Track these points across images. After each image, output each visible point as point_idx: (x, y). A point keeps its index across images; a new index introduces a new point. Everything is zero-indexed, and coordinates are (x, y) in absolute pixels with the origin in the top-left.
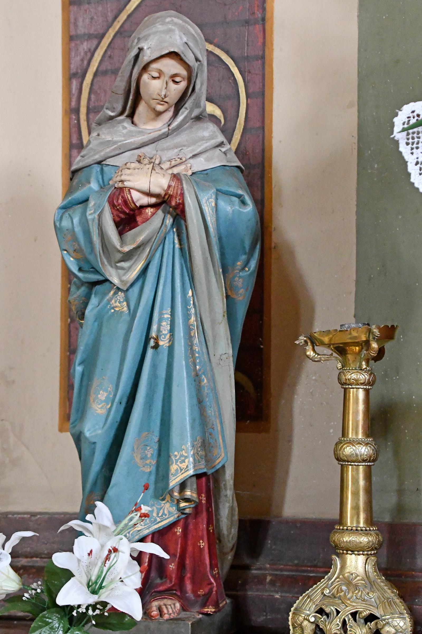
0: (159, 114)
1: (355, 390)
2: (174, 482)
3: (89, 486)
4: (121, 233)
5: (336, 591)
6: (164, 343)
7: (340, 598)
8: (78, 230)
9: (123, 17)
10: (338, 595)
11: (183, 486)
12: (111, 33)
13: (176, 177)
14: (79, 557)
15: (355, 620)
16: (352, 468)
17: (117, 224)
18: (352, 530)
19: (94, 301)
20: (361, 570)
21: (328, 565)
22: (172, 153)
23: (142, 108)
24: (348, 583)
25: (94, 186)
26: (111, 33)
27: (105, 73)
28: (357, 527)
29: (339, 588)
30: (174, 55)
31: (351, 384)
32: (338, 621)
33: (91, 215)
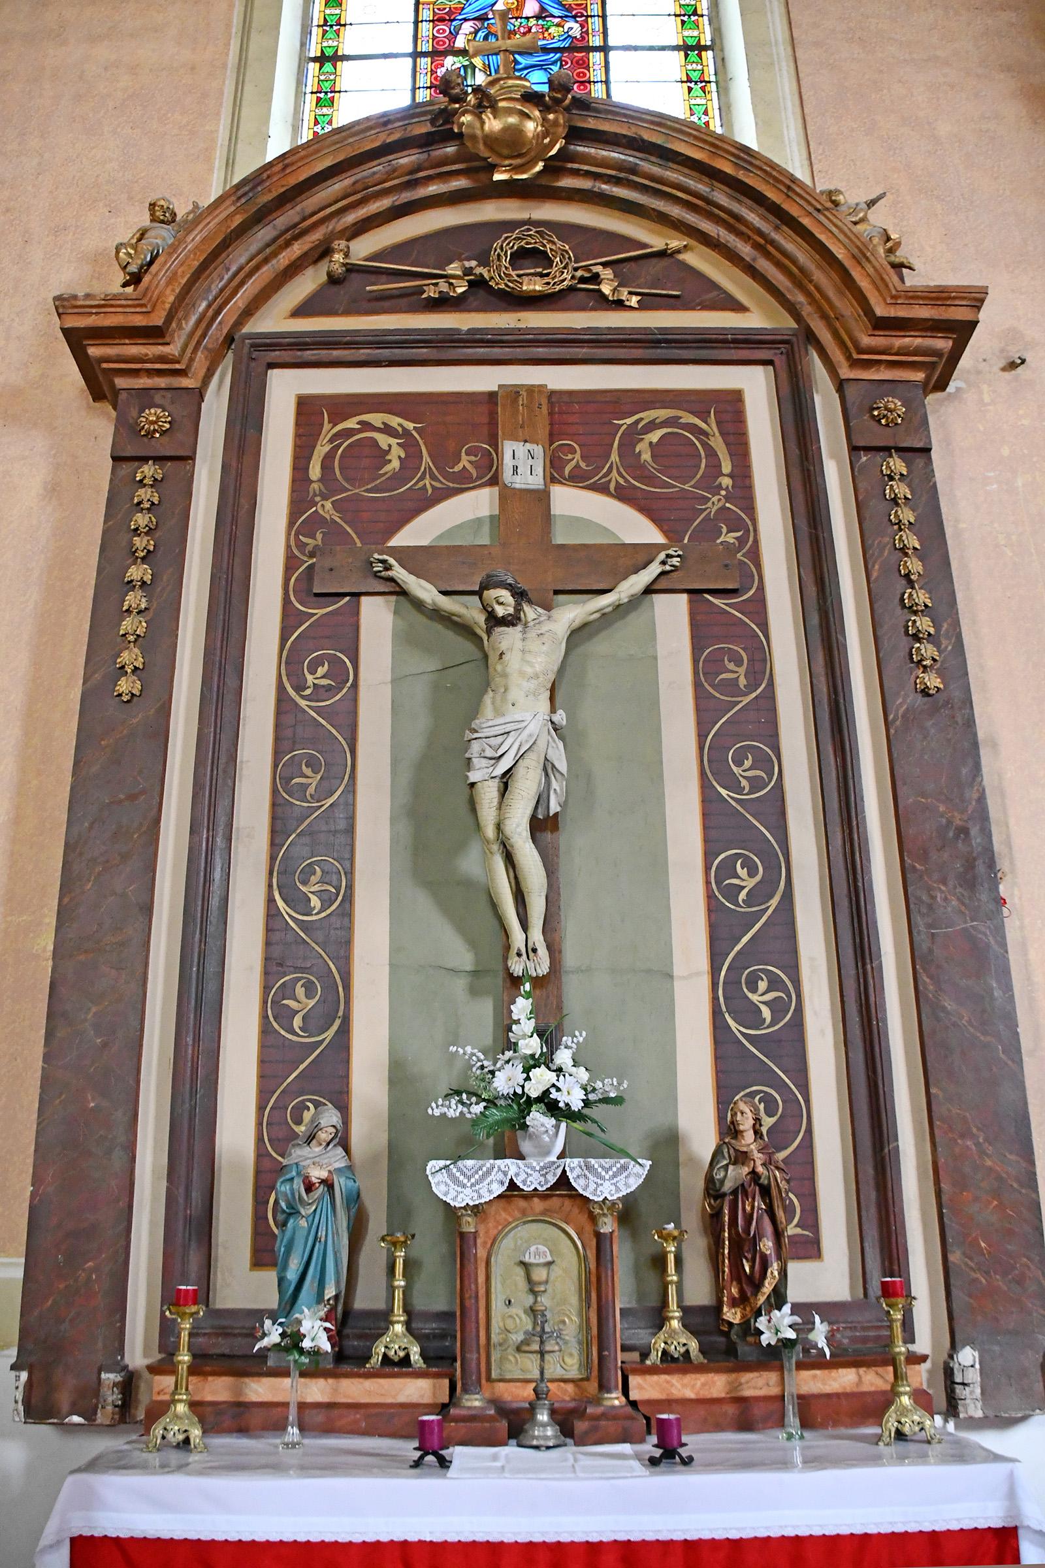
0: (321, 1144)
2: (326, 1298)
3: (284, 1303)
4: (307, 1193)
6: (323, 1240)
8: (288, 1192)
9: (285, 1084)
11: (329, 1300)
12: (279, 1092)
13: (330, 1171)
17: (306, 1190)
19: (291, 1221)
20: (400, 1331)
21: (388, 1329)
22: (326, 1161)
23: (314, 1142)
24: (397, 1335)
25: (294, 1173)
26: (279, 1092)
27: (275, 1108)
30: (333, 1126)
33: (295, 1186)
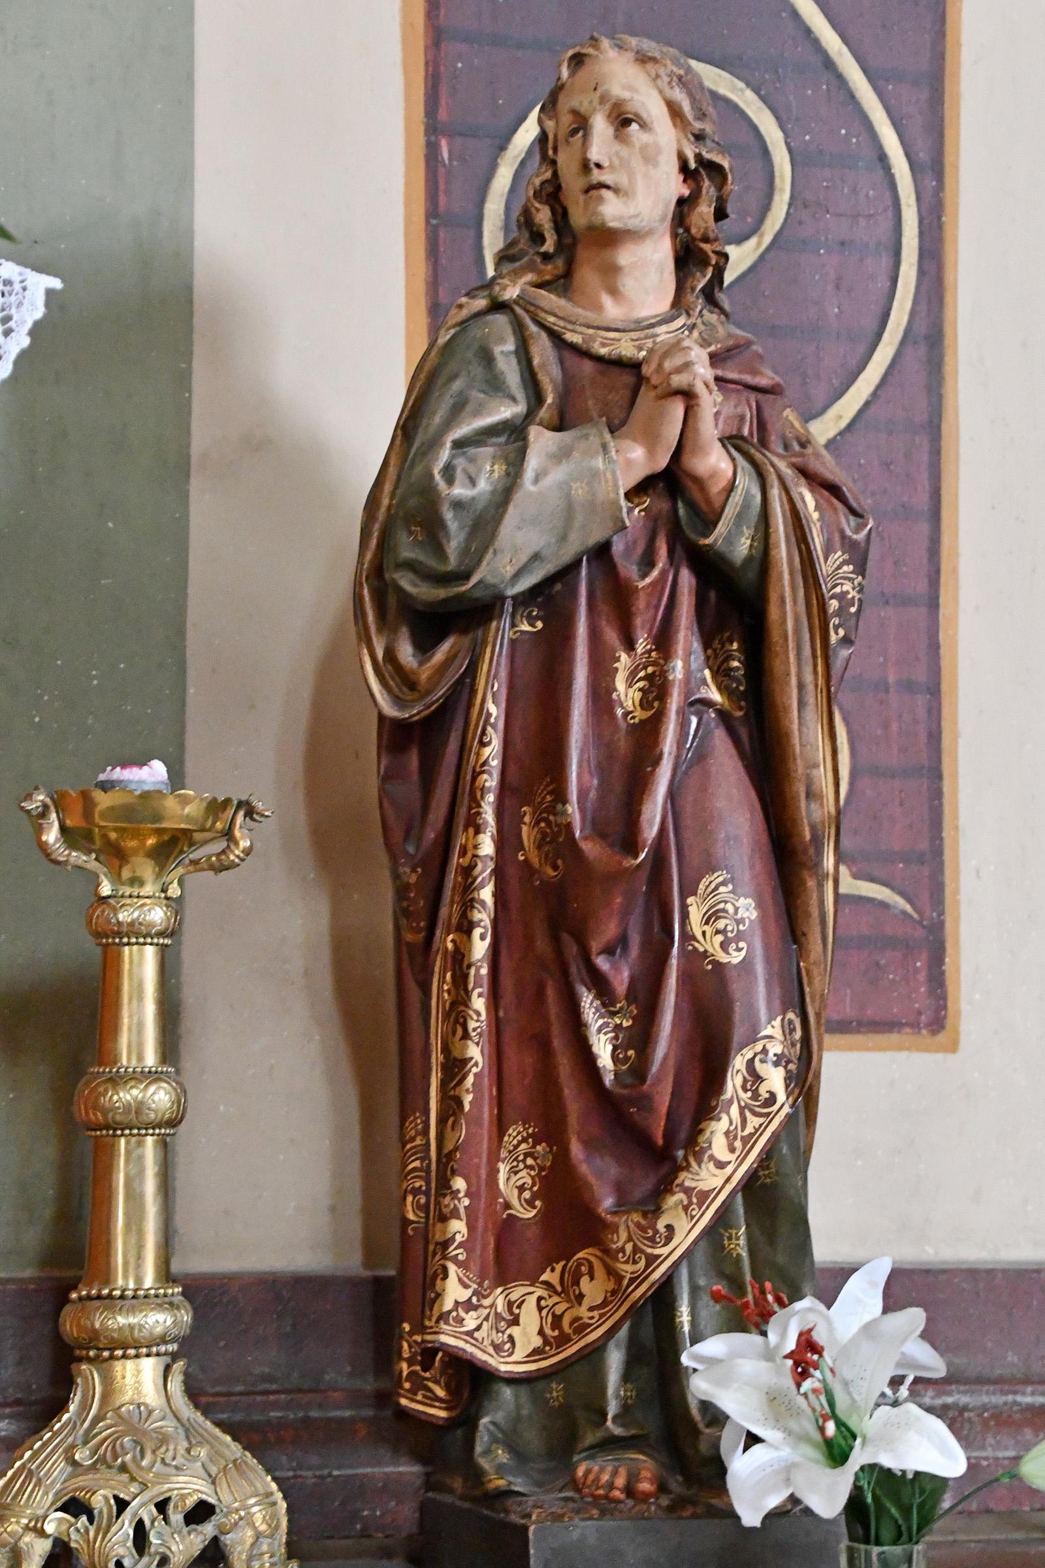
1: (135, 948)
5: (110, 1448)
7: (123, 1468)
10: (120, 1460)
14: (683, 1214)
15: (166, 1520)
16: (127, 1143)
18: (146, 1297)
28: (136, 1290)
29: (118, 1442)
31: (119, 934)
32: (125, 1528)
